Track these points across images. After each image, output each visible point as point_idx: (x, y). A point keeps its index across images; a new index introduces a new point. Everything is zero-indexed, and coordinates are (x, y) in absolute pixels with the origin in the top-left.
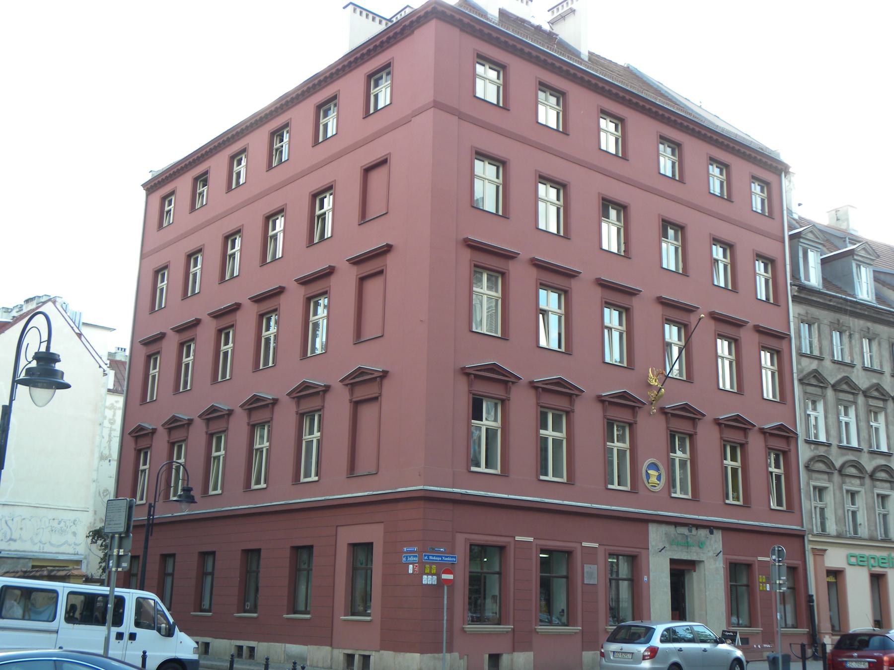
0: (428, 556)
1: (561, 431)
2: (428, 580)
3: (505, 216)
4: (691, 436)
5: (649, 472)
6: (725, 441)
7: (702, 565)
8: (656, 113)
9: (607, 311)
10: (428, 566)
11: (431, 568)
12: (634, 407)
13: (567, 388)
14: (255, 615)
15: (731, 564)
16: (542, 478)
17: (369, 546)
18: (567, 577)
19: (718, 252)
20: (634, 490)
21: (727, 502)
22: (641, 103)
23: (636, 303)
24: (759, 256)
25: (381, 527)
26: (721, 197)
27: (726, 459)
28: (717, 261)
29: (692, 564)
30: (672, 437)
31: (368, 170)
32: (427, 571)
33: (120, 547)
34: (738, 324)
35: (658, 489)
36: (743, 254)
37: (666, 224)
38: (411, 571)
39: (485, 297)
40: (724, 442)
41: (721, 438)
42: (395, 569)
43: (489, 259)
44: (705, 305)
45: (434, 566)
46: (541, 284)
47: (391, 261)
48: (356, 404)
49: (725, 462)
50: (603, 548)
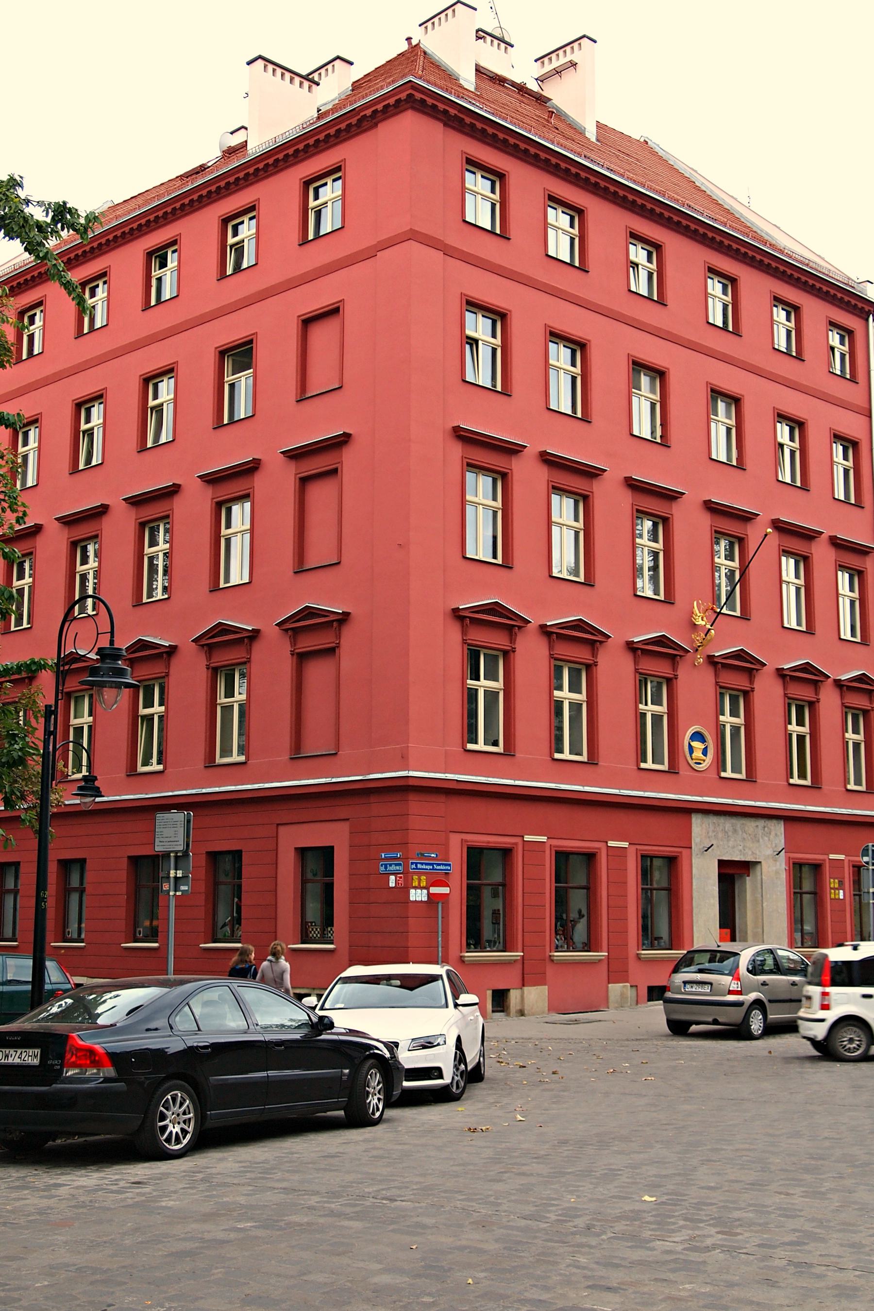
0: (416, 864)
1: (580, 692)
2: (417, 895)
3: (506, 393)
4: (589, 667)
5: (693, 744)
6: (789, 698)
7: (758, 867)
8: (557, 165)
9: (555, 499)
10: (415, 877)
11: (419, 880)
12: (818, 681)
13: (511, 619)
14: (156, 945)
15: (469, 848)
16: (470, 746)
17: (327, 854)
18: (587, 888)
19: (783, 433)
20: (673, 770)
21: (723, 774)
22: (684, 222)
23: (679, 513)
24: (838, 437)
25: (345, 827)
26: (788, 354)
27: (790, 723)
28: (781, 446)
29: (746, 867)
30: (642, 683)
31: (308, 322)
32: (415, 884)
33: (176, 869)
34: (809, 536)
35: (703, 766)
36: (817, 436)
37: (638, 366)
38: (392, 884)
39: (646, 550)
40: (789, 700)
41: (785, 695)
42: (368, 885)
43: (488, 453)
44: (767, 510)
45: (423, 878)
46: (554, 488)
47: (350, 460)
48: (302, 658)
49: (721, 718)
50: (634, 848)
